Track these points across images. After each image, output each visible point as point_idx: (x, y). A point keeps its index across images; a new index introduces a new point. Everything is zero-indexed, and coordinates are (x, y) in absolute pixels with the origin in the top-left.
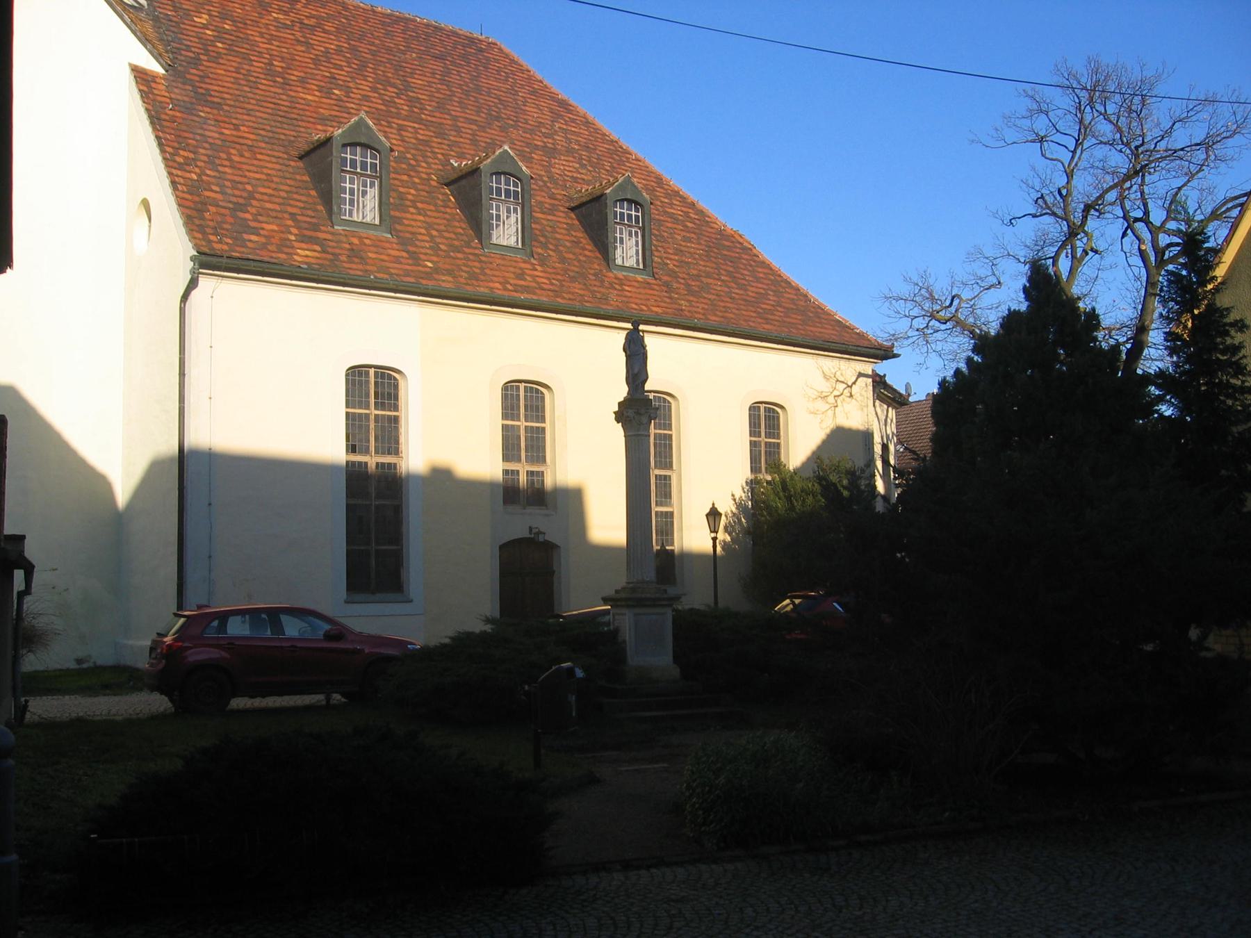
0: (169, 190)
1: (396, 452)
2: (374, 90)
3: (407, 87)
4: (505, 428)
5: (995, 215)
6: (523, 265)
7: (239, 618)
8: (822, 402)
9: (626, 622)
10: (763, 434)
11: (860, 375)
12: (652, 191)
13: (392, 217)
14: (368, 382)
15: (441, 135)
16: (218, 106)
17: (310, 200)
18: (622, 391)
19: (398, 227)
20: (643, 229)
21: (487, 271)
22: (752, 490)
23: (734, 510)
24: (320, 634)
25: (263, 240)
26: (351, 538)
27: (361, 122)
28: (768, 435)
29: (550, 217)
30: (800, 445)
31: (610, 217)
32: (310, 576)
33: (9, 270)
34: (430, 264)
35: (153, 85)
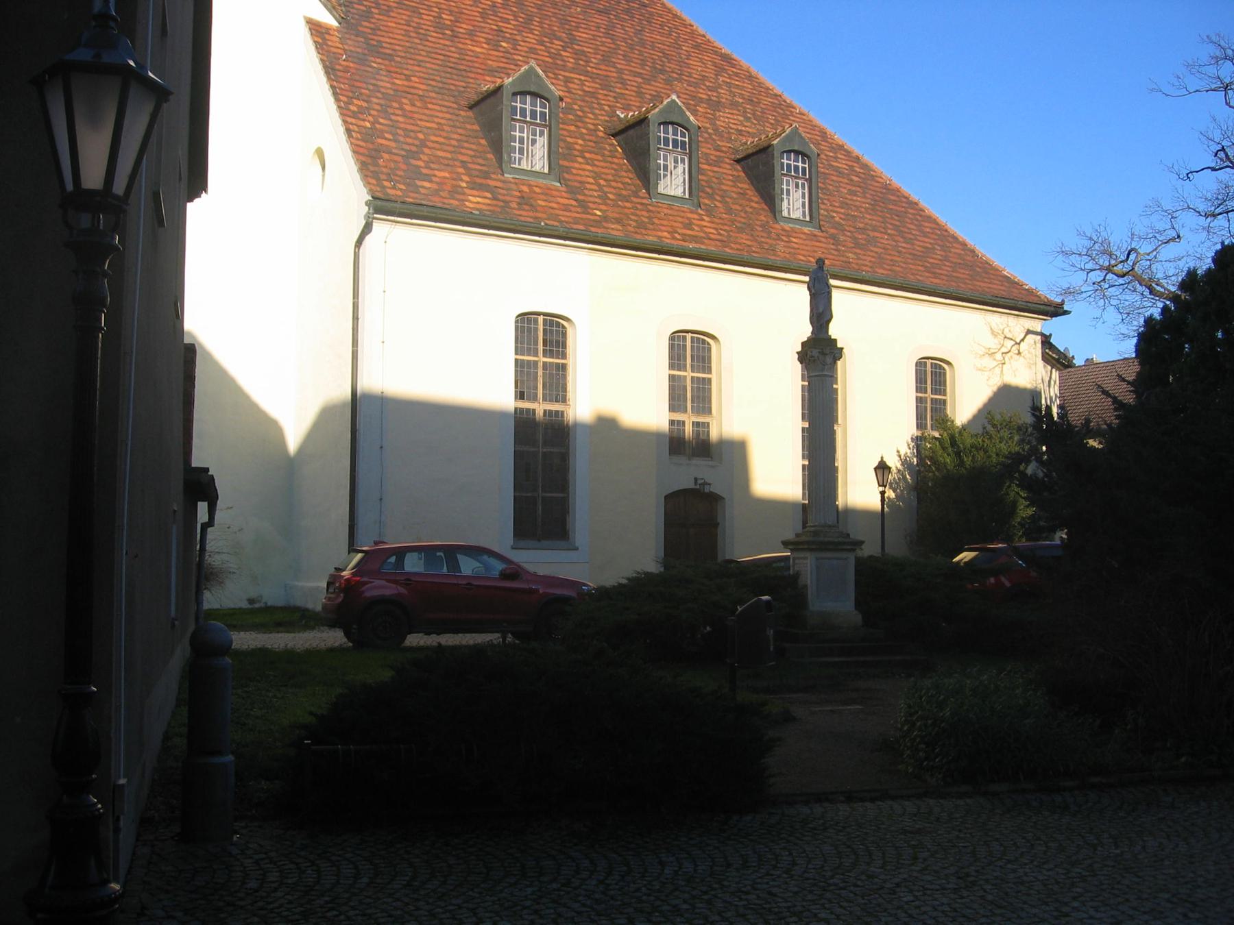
0: (344, 137)
1: (564, 400)
2: (541, 43)
3: (573, 40)
4: (672, 378)
5: (1170, 169)
6: (689, 215)
7: (415, 555)
8: (991, 360)
9: (807, 566)
10: (929, 390)
11: (1029, 332)
12: (817, 144)
13: (561, 166)
14: (536, 329)
15: (605, 86)
16: (389, 57)
17: (480, 149)
18: (806, 331)
19: (566, 176)
20: (810, 181)
21: (656, 221)
22: (918, 447)
23: (899, 466)
24: (496, 573)
25: (435, 186)
26: (517, 487)
27: (531, 71)
28: (934, 392)
29: (716, 169)
30: (966, 404)
31: (777, 168)
32: (481, 516)
33: (204, 195)
34: (598, 213)
35: (327, 37)
